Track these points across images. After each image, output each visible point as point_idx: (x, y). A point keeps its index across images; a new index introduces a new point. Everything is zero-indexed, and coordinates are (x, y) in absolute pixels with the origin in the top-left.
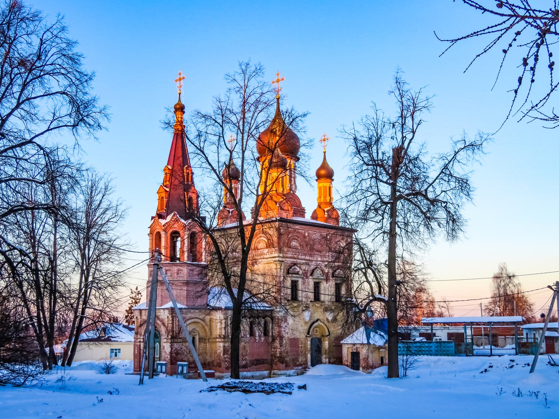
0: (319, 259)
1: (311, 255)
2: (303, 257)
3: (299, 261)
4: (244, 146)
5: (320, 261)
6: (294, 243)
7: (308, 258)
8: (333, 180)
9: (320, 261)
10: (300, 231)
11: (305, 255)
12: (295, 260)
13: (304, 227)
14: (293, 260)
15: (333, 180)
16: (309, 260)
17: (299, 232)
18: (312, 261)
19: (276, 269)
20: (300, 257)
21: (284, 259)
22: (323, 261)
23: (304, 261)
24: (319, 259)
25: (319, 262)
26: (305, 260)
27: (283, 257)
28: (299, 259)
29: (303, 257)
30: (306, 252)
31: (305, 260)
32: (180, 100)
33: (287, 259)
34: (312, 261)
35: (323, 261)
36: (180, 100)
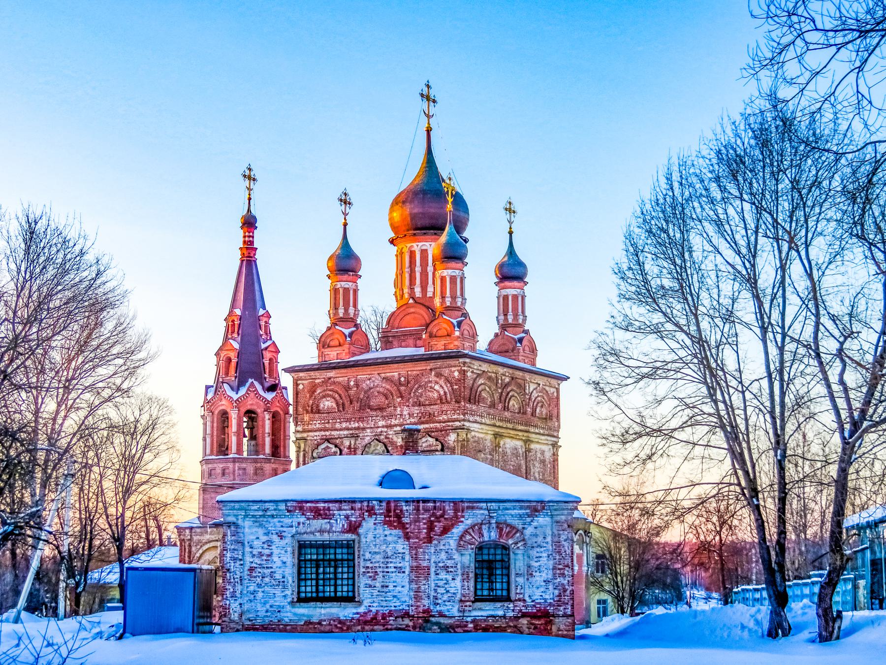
0: (381, 423)
1: (361, 419)
2: (344, 425)
3: (335, 433)
4: (821, 46)
5: (383, 427)
6: (327, 403)
7: (357, 425)
8: (526, 283)
9: (383, 427)
10: (338, 380)
11: (348, 420)
12: (327, 433)
13: (343, 371)
14: (323, 433)
15: (526, 283)
16: (358, 428)
17: (334, 383)
18: (364, 429)
19: (305, 567)
20: (338, 426)
21: (305, 435)
22: (390, 426)
23: (346, 432)
24: (381, 423)
25: (380, 430)
26: (348, 429)
27: (304, 431)
28: (337, 430)
29: (344, 425)
30: (349, 416)
31: (351, 429)
32: (249, 210)
33: (310, 434)
34: (364, 429)
35: (390, 426)
36: (249, 210)
